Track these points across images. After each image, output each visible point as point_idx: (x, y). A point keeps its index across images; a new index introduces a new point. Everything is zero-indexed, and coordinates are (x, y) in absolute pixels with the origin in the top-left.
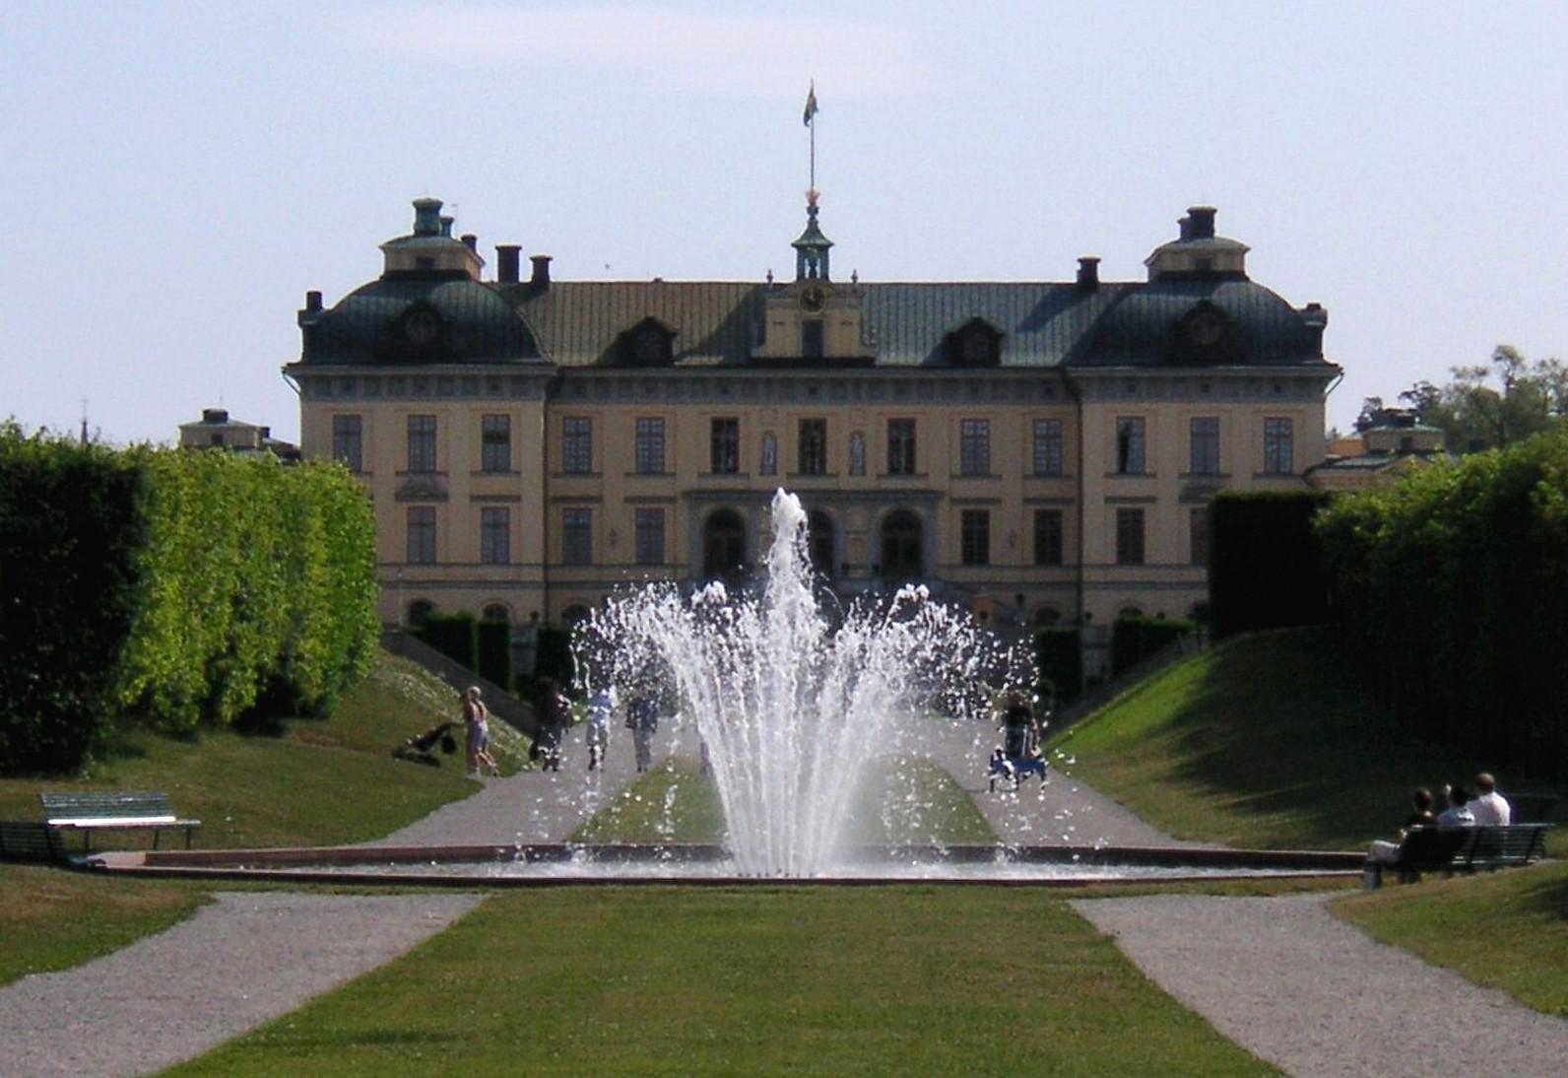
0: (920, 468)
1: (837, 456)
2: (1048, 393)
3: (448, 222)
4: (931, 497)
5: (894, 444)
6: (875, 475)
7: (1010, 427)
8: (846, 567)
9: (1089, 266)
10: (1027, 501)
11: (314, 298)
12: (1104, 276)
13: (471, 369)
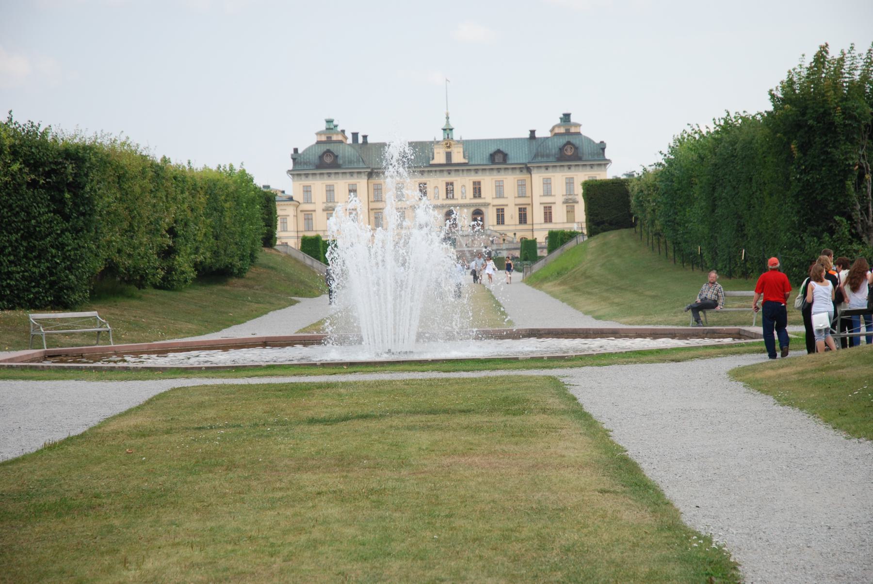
0: (483, 195)
1: (457, 193)
2: (521, 170)
3: (336, 126)
4: (487, 205)
5: (475, 189)
7: (510, 180)
9: (533, 132)
11: (296, 150)
12: (537, 135)
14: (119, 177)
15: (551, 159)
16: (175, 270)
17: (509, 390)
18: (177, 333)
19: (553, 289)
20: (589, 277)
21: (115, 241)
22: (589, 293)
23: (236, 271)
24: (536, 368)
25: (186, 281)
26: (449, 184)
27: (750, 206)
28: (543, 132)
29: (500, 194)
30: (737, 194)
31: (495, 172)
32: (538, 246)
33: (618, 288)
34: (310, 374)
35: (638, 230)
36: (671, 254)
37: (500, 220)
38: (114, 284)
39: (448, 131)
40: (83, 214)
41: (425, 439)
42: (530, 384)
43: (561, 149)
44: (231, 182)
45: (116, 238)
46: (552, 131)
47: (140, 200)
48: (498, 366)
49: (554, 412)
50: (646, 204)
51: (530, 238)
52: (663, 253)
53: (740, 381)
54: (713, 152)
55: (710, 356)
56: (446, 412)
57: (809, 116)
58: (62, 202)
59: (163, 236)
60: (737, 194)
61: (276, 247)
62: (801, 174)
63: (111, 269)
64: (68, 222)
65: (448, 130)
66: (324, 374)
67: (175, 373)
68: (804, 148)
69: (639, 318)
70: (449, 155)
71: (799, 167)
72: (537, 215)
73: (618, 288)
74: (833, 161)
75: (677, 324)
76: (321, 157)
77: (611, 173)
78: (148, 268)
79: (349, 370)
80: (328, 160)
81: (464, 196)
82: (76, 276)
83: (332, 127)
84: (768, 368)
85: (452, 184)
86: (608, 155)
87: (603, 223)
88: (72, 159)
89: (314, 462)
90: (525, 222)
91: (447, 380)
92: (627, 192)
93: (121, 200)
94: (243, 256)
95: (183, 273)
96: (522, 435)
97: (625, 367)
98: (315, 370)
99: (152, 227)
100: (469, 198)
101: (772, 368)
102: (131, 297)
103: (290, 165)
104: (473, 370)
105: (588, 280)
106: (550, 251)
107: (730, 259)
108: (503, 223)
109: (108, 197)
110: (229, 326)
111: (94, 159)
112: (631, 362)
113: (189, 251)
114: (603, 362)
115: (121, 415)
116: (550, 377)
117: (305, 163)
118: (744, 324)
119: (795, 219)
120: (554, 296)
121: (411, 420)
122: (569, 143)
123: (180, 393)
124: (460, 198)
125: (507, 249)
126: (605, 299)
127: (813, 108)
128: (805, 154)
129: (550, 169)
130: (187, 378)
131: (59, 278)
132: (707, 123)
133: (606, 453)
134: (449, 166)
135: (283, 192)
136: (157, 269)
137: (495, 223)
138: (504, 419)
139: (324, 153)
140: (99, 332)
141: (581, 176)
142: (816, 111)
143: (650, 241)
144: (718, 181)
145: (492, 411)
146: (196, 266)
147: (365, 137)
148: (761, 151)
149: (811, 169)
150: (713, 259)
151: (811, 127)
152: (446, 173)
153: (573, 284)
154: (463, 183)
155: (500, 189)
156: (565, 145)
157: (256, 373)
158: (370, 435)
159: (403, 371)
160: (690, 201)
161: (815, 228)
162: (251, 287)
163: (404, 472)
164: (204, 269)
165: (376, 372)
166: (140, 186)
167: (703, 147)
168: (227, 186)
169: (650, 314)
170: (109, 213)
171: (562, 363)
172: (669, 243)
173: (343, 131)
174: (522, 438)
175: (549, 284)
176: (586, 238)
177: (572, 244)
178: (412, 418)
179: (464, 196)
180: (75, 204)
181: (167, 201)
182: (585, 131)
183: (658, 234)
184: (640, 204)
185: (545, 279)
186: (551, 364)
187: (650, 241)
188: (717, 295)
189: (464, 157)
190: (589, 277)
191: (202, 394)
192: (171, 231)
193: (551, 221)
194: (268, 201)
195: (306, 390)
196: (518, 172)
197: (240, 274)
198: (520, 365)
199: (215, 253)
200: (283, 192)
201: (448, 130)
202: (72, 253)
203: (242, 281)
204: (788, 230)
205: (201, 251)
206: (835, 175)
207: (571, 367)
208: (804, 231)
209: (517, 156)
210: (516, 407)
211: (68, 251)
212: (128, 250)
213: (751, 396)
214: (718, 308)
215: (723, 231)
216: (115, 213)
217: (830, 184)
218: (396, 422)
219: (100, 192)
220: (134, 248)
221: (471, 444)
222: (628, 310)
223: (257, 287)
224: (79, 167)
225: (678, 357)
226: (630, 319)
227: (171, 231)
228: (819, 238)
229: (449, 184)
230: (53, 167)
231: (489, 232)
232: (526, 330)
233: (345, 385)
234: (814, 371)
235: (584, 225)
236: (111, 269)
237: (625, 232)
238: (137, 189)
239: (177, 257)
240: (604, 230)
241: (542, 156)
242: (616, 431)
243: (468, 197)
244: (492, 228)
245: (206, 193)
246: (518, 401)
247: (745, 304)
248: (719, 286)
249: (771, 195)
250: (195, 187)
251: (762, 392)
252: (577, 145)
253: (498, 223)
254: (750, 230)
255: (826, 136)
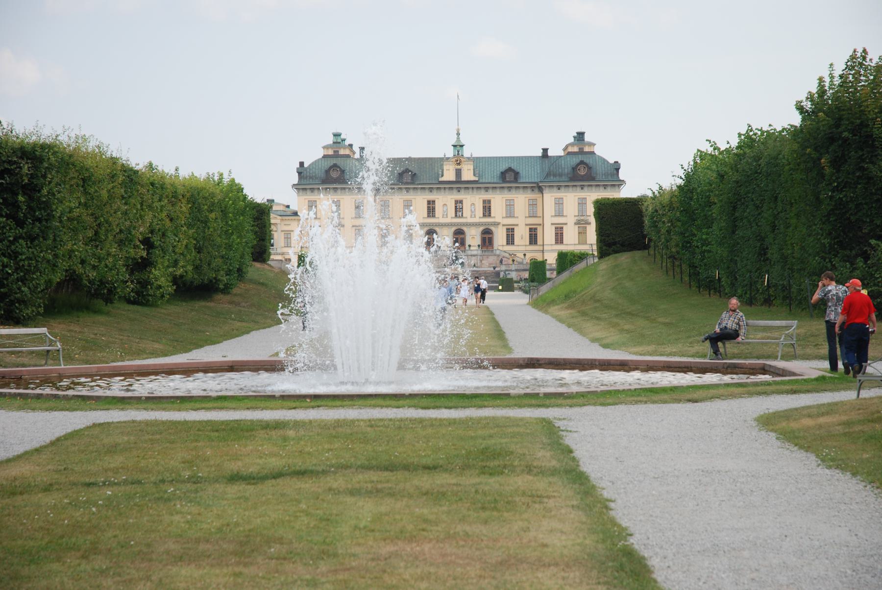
0: (492, 215)
1: (467, 211)
2: (532, 189)
3: (344, 140)
4: (497, 224)
5: (484, 207)
6: (450, 218)
7: (521, 200)
8: (470, 246)
9: (545, 151)
10: (527, 225)
11: (302, 164)
12: (550, 153)
13: (335, 186)
14: (84, 180)
15: (563, 178)
16: (152, 284)
17: (491, 436)
18: (140, 353)
19: (559, 313)
20: (598, 301)
21: (78, 251)
22: (598, 319)
23: (221, 286)
24: (531, 406)
25: (163, 296)
26: (458, 202)
27: (774, 227)
28: (556, 151)
29: (510, 214)
30: (759, 214)
31: (506, 191)
32: (548, 267)
33: (630, 314)
34: (266, 408)
35: (652, 252)
36: (687, 279)
37: (510, 240)
38: (75, 297)
39: (458, 148)
40: (39, 220)
41: (366, 509)
42: (516, 429)
43: (574, 169)
44: (218, 191)
45: (80, 248)
46: (565, 150)
47: (108, 206)
48: (486, 403)
49: (542, 472)
50: (660, 225)
51: (540, 259)
52: (678, 277)
53: (772, 431)
54: (735, 168)
55: (733, 396)
56: (406, 468)
57: (843, 127)
58: (16, 205)
59: (136, 247)
60: (759, 214)
61: (269, 262)
62: (833, 192)
63: (72, 280)
64: (22, 228)
65: (458, 146)
66: (282, 408)
67: (109, 403)
68: (836, 163)
69: (651, 348)
70: (458, 173)
71: (831, 184)
72: (549, 236)
73: (630, 314)
74: (870, 178)
75: (693, 356)
76: (327, 172)
77: (628, 192)
78: (116, 281)
79: (313, 404)
80: (334, 174)
81: (473, 215)
82: (29, 288)
83: (339, 140)
84: (804, 416)
85: (461, 202)
86: (622, 176)
87: (615, 244)
88: (28, 158)
89: (208, 546)
90: (536, 243)
91: (421, 421)
92: (641, 211)
93: (86, 206)
94: (230, 270)
95: (160, 287)
96: (495, 509)
97: (633, 408)
98: (273, 403)
99: (122, 236)
100: (478, 217)
101: (809, 416)
102: (97, 312)
103: (295, 179)
104: (456, 407)
105: (597, 305)
106: (559, 273)
107: (751, 285)
108: (513, 243)
109: (70, 201)
110: (201, 346)
111: (53, 159)
112: (641, 401)
113: (166, 264)
114: (610, 401)
115: (19, 458)
116: (544, 419)
117: (311, 178)
118: (768, 357)
119: (826, 241)
120: (561, 320)
121: (361, 479)
122: (582, 162)
123: (96, 431)
124: (469, 216)
125: (516, 270)
126: (615, 325)
127: (848, 119)
128: (838, 171)
129: (563, 189)
130: (122, 409)
131: (10, 290)
132: (728, 139)
133: (604, 541)
134: (459, 184)
135: (288, 207)
136: (127, 282)
137: (505, 243)
138: (477, 480)
139: (331, 167)
140: (48, 351)
141: (593, 195)
142: (852, 123)
143: (664, 264)
144: (740, 200)
145: (465, 467)
146: (175, 280)
147: (362, 149)
148: (787, 167)
149: (845, 187)
150: (733, 285)
151: (846, 140)
152: (455, 191)
153: (581, 308)
154: (473, 201)
155: (511, 209)
156: (578, 165)
157: (203, 405)
158: (299, 502)
159: (375, 406)
160: (709, 223)
161: (848, 252)
162: (238, 304)
163: (323, 567)
164: (184, 284)
165: (343, 406)
166: (109, 191)
167: (725, 164)
168: (212, 195)
169: (663, 344)
170: (70, 219)
171: (560, 401)
172: (684, 267)
173: (351, 146)
174: (495, 513)
175: (556, 307)
176: (596, 260)
177: (582, 265)
178: (361, 477)
179: (473, 215)
180: (30, 208)
181: (142, 209)
182: (599, 151)
183: (672, 257)
184: (654, 225)
185: (553, 302)
186: (548, 402)
187: (664, 264)
188: (738, 324)
189: (474, 175)
190: (598, 301)
191: (122, 433)
192: (147, 243)
193: (562, 242)
194: (260, 215)
195: (247, 431)
196: (529, 191)
197: (226, 290)
198: (512, 402)
199: (197, 268)
200: (288, 207)
201: (458, 146)
202: (26, 263)
203: (227, 298)
204: (818, 253)
205: (181, 263)
206: (872, 194)
207: (571, 406)
208: (836, 256)
209: (529, 175)
210: (496, 463)
211: (21, 260)
212: (94, 262)
213: (787, 452)
214: (740, 339)
215: (744, 254)
216: (78, 219)
217: (866, 204)
218: (338, 482)
219: (58, 196)
220: (100, 259)
221: (426, 521)
222: (639, 339)
223: (243, 304)
224: (36, 168)
225: (695, 396)
226: (641, 349)
227: (147, 243)
228: (852, 264)
229: (458, 202)
230: (6, 166)
231: (498, 252)
232: (524, 359)
233: (297, 424)
234: (861, 422)
235: (595, 247)
236: (72, 280)
237: (638, 254)
238: (104, 194)
239: (153, 270)
240: (616, 252)
241: (555, 175)
242: (619, 502)
243: (477, 217)
244: (500, 248)
245: (188, 202)
246: (499, 454)
247: (769, 334)
248: (741, 314)
249: (798, 215)
250: (175, 195)
251: (801, 447)
252: (591, 165)
253: (508, 243)
254: (773, 253)
255: (862, 150)
